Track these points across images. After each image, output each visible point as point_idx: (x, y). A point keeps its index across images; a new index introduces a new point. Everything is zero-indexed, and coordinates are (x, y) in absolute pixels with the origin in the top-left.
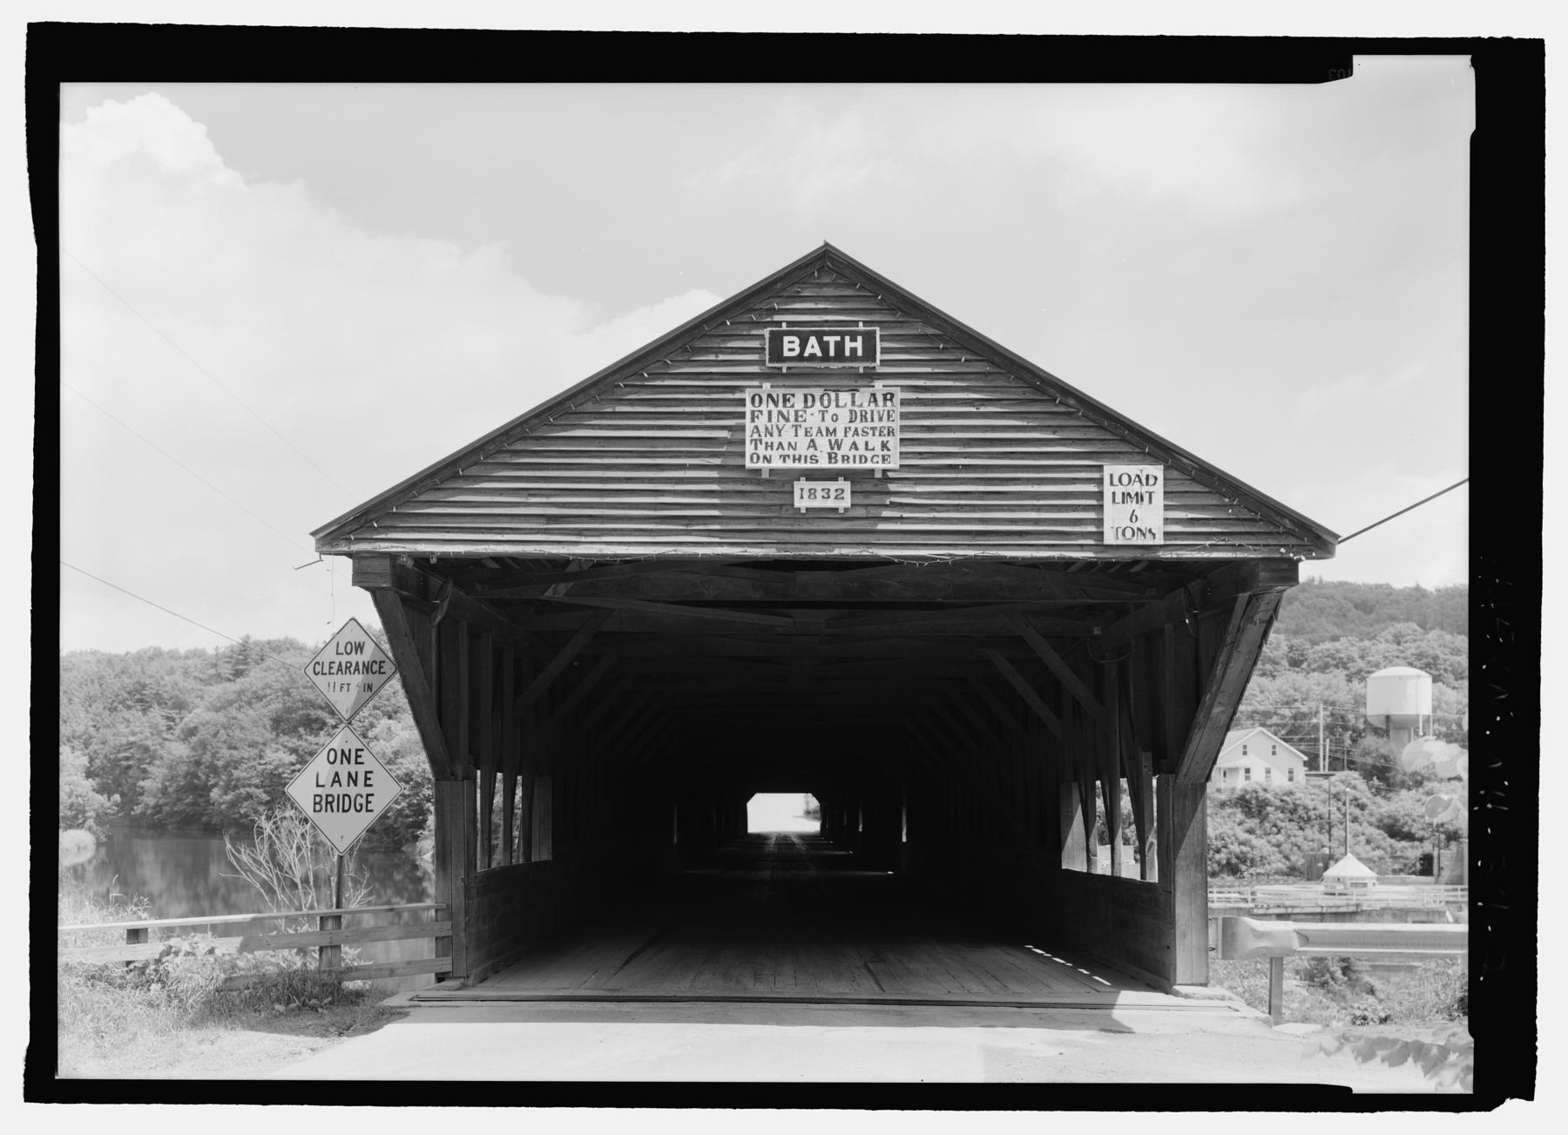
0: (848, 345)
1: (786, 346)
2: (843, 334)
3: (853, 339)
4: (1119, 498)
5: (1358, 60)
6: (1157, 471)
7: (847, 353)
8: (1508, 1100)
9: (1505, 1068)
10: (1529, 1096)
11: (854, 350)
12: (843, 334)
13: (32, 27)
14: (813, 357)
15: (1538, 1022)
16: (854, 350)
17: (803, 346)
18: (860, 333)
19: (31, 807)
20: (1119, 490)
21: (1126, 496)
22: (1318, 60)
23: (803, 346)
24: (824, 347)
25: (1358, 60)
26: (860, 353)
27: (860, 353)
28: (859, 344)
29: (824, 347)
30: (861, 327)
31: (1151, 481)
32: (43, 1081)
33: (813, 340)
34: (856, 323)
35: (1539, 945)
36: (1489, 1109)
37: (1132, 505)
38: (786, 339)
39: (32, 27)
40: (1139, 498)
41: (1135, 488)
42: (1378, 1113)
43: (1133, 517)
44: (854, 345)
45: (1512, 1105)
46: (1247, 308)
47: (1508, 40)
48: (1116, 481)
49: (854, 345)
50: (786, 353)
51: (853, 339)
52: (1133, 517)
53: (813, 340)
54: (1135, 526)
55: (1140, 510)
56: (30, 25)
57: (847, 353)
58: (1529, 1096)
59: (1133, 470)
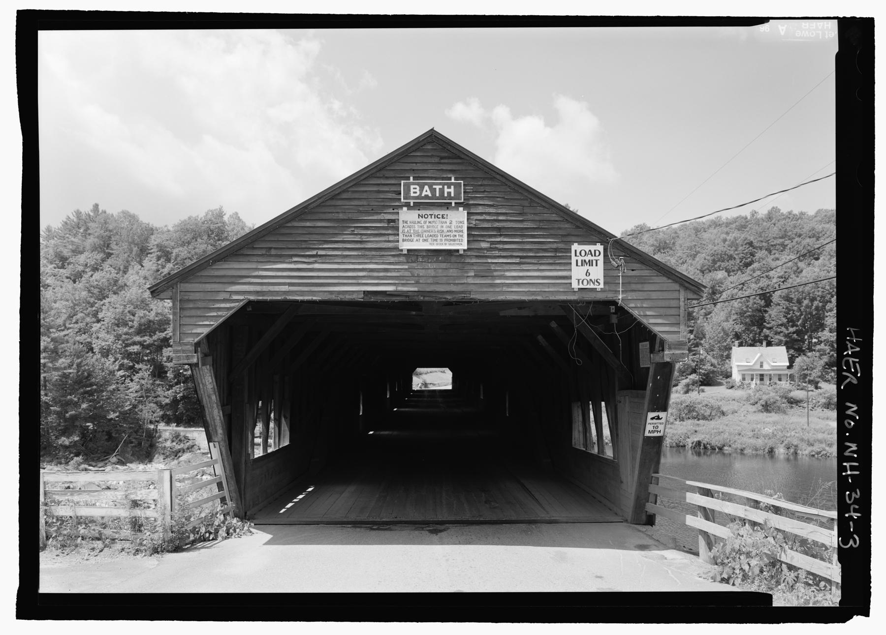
0: (446, 190)
1: (412, 190)
2: (444, 185)
3: (449, 187)
4: (580, 264)
6: (600, 247)
7: (446, 195)
9: (856, 599)
10: (866, 614)
11: (449, 193)
12: (444, 185)
13: (19, 12)
14: (427, 197)
15: (872, 572)
16: (449, 193)
17: (421, 190)
18: (452, 184)
19: (20, 540)
20: (580, 259)
21: (584, 262)
23: (421, 190)
24: (433, 191)
26: (452, 195)
27: (452, 195)
28: (452, 190)
29: (433, 191)
30: (453, 181)
31: (597, 253)
32: (32, 603)
33: (426, 187)
34: (450, 179)
35: (872, 529)
36: (844, 622)
37: (586, 267)
38: (412, 187)
39: (19, 12)
40: (590, 263)
41: (588, 258)
43: (588, 273)
44: (449, 190)
45: (857, 619)
46: (659, 154)
47: (853, 18)
48: (578, 254)
49: (449, 190)
50: (412, 195)
51: (449, 187)
52: (588, 273)
53: (426, 187)
54: (588, 278)
55: (592, 269)
56: (18, 11)
57: (446, 195)
58: (866, 614)
59: (587, 248)
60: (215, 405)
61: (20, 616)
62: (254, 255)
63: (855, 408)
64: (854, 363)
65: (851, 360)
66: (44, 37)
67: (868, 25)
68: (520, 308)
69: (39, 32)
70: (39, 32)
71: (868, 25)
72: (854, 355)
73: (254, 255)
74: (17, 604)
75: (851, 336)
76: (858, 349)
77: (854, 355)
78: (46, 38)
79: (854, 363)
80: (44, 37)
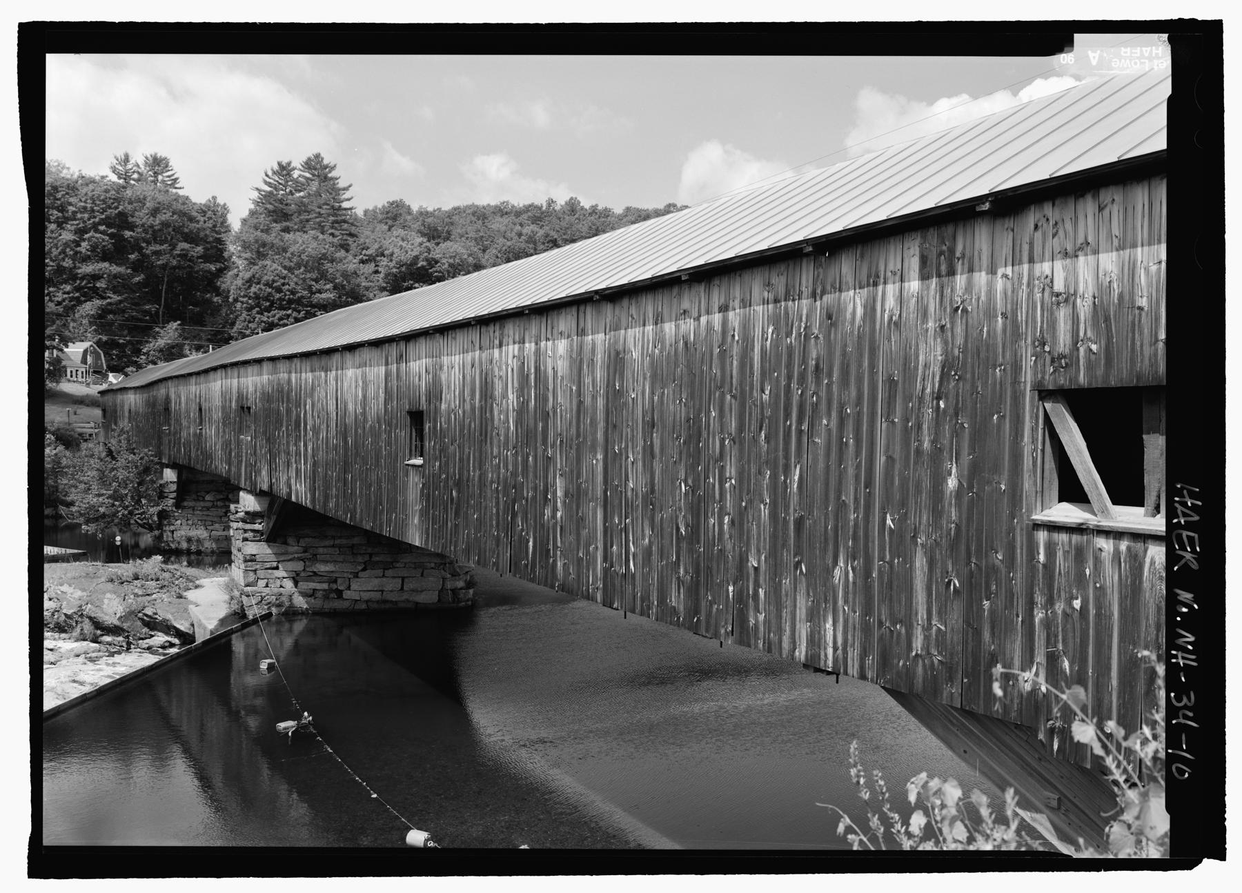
5: (1078, 38)
8: (1205, 860)
10: (1221, 856)
13: (21, 25)
15: (1226, 236)
22: (1047, 38)
25: (1078, 38)
36: (1191, 869)
39: (21, 25)
42: (1103, 872)
47: (1193, 21)
56: (1221, 21)
58: (1221, 856)
60: (676, 710)
61: (31, 874)
62: (1012, 750)
63: (1192, 639)
64: (1190, 539)
65: (1185, 534)
66: (54, 62)
67: (1214, 29)
68: (653, 456)
69: (49, 57)
70: (49, 57)
71: (1214, 29)
72: (1189, 526)
73: (1012, 750)
74: (29, 857)
75: (1182, 496)
76: (1196, 518)
77: (1189, 526)
78: (57, 66)
79: (1190, 539)
80: (54, 62)
